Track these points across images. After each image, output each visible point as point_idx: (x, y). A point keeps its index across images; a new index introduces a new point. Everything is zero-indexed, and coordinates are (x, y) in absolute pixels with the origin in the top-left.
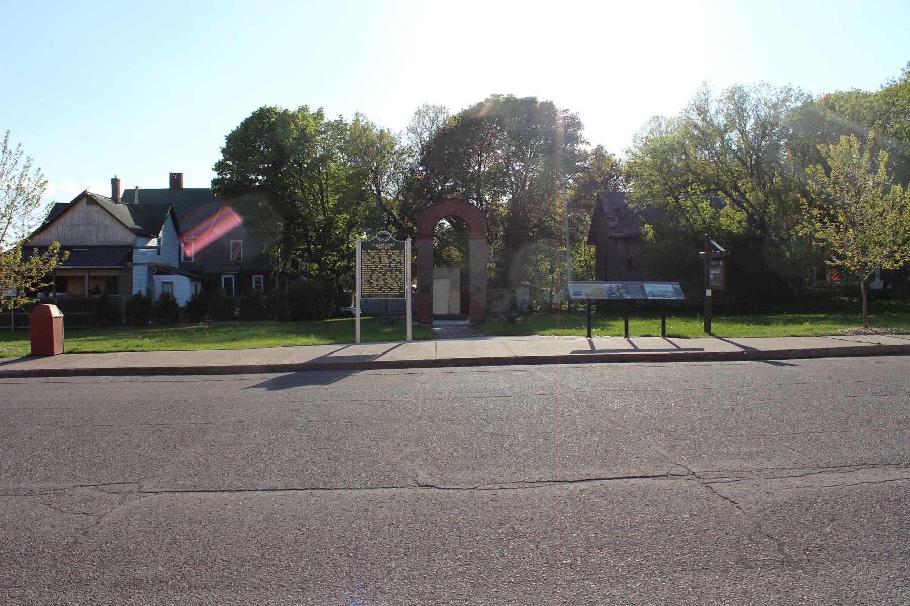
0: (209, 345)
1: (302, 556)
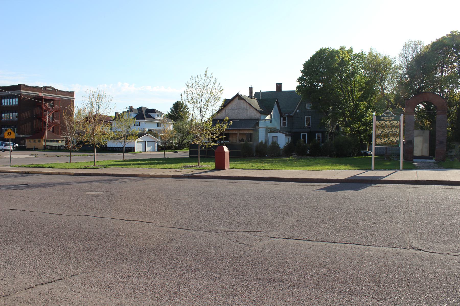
0: (296, 168)
1: (350, 278)
